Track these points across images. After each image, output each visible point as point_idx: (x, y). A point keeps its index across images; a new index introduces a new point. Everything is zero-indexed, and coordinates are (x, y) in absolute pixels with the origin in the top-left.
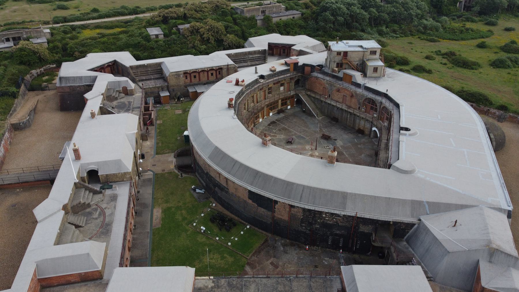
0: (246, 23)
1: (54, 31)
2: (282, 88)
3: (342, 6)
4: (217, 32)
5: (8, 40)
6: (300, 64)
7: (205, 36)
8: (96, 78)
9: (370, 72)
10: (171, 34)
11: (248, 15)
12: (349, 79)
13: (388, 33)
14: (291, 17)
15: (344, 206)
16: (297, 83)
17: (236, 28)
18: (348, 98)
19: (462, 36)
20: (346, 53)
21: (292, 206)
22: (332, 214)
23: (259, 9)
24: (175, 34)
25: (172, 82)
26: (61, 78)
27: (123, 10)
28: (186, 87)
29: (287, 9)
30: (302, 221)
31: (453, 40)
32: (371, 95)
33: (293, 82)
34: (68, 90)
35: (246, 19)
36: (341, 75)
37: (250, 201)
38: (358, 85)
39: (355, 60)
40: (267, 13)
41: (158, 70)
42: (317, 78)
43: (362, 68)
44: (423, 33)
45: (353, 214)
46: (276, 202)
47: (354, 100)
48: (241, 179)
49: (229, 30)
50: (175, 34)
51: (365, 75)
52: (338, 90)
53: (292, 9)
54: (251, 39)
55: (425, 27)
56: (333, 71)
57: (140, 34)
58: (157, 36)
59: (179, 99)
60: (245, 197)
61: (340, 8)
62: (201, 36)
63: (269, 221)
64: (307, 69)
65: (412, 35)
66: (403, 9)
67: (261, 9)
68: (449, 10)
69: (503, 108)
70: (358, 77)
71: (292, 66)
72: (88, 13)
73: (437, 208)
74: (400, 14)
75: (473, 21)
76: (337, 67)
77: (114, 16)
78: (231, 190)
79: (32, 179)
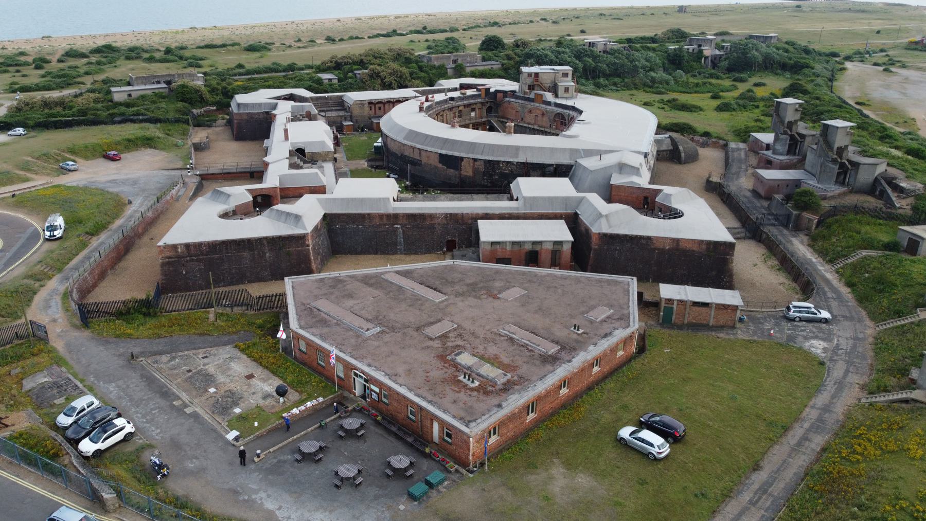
0: (434, 71)
1: (208, 78)
2: (473, 114)
3: (549, 53)
4: (401, 77)
5: (158, 82)
6: (492, 90)
7: (387, 80)
8: (277, 104)
9: (561, 92)
10: (346, 78)
11: (437, 64)
12: (539, 99)
13: (606, 86)
14: (490, 67)
15: (517, 156)
16: (489, 110)
17: (423, 74)
18: (540, 117)
19: (698, 89)
20: (537, 74)
21: (475, 160)
22: (508, 162)
23: (449, 57)
24: (351, 78)
25: (356, 112)
26: (239, 105)
27: (26, 281)
28: (370, 118)
29: (484, 59)
30: (484, 174)
31: (684, 92)
32: (560, 110)
33: (485, 109)
34: (245, 117)
35: (434, 67)
36: (532, 96)
37: (440, 166)
38: (549, 103)
39: (546, 81)
40: (459, 62)
41: (340, 104)
42: (509, 102)
43: (554, 89)
44: (650, 87)
45: (523, 161)
46: (462, 159)
47: (545, 119)
48: (433, 147)
49: (414, 75)
50: (351, 78)
51: (557, 96)
52: (530, 112)
53: (490, 59)
54: (440, 82)
55: (653, 80)
56: (525, 93)
57: (311, 79)
58: (330, 80)
59: (362, 130)
60: (435, 161)
61: (546, 56)
62: (382, 80)
63: (457, 181)
64: (499, 95)
65: (636, 88)
66: (626, 61)
67: (452, 58)
68: (691, 67)
69: (707, 134)
70: (549, 96)
71: (484, 92)
72: (232, 69)
73: (589, 153)
74: (622, 66)
75: (718, 78)
76: (529, 89)
77: (266, 72)
78: (424, 160)
79: (234, 171)
